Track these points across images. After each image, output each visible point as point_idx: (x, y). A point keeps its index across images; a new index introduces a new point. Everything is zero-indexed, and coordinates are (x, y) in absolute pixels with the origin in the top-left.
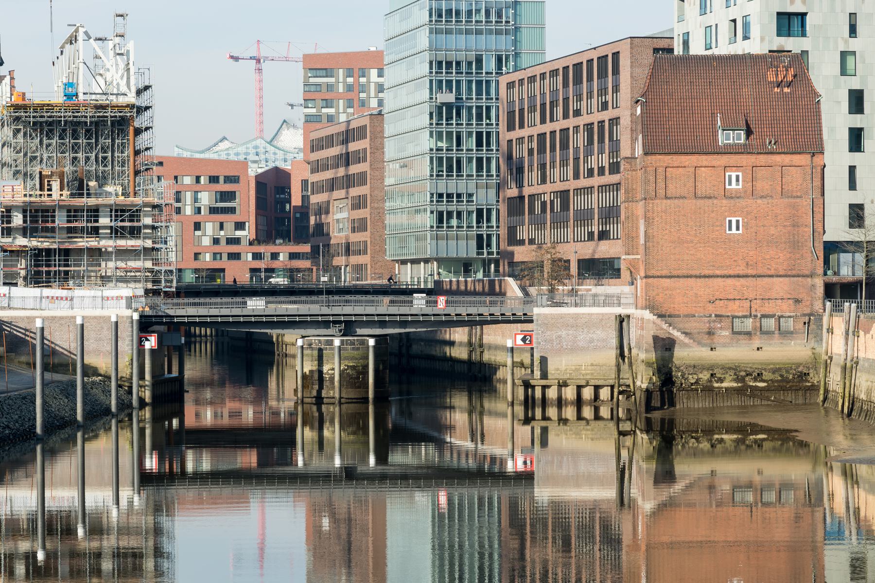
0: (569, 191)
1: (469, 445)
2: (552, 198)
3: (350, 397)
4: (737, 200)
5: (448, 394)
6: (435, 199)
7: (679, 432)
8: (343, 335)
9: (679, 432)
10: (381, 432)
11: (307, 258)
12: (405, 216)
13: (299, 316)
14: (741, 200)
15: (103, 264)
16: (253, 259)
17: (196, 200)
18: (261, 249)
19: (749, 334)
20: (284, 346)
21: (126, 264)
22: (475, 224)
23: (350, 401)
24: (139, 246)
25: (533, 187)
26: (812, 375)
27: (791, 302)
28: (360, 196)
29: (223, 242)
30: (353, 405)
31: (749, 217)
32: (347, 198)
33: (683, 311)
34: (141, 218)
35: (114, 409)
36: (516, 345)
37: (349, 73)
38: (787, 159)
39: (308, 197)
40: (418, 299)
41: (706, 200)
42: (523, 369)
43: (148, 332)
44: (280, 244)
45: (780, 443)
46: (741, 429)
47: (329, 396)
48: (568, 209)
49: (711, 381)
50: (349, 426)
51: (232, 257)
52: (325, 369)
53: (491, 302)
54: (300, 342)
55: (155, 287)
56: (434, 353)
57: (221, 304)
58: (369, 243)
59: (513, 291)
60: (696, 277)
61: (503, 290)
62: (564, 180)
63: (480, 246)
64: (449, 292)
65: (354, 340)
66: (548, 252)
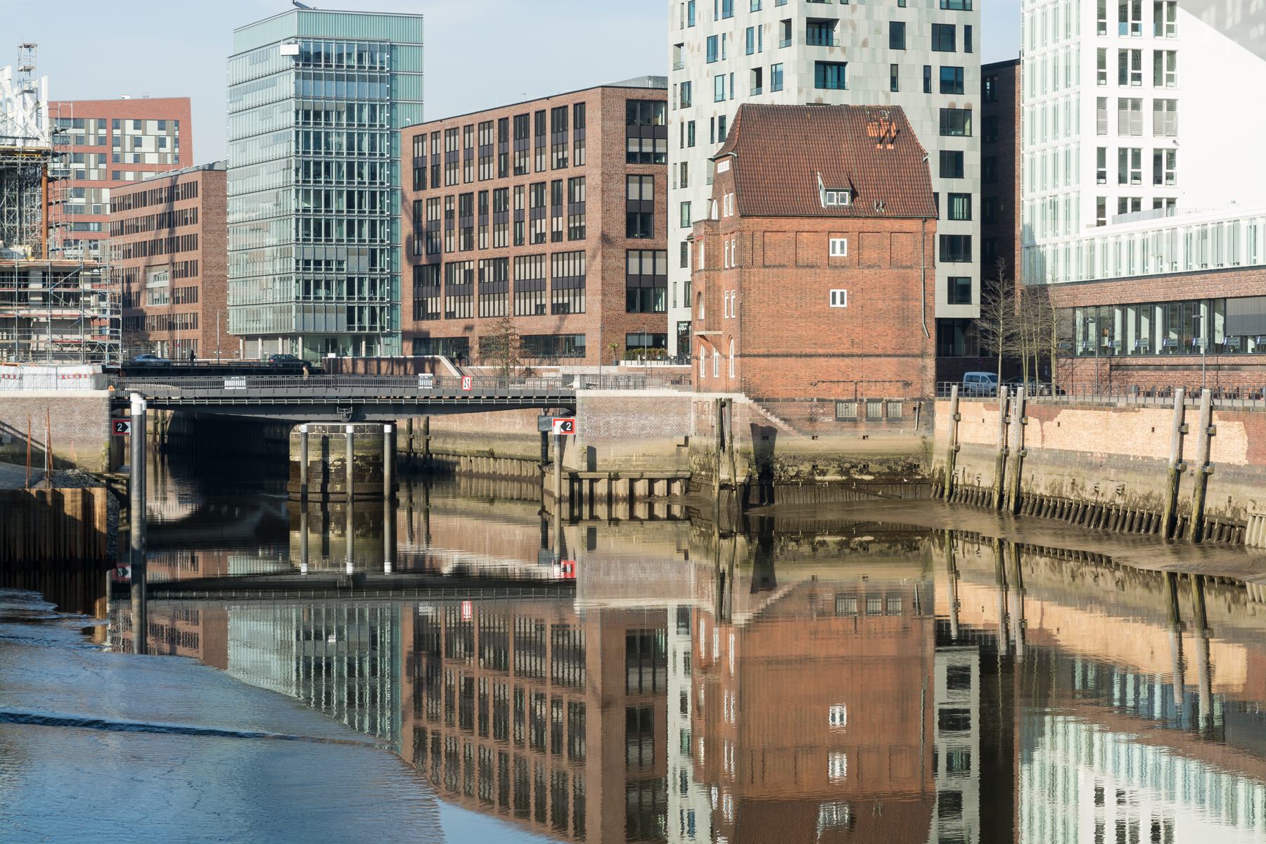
4: (842, 270)
6: (301, 266)
7: (777, 533)
9: (777, 533)
13: (235, 398)
14: (846, 270)
15: (34, 337)
19: (854, 420)
26: (922, 467)
27: (900, 385)
28: (186, 262)
31: (855, 289)
33: (781, 392)
37: (102, 124)
38: (896, 225)
40: (424, 379)
41: (808, 270)
45: (887, 545)
46: (847, 530)
49: (812, 474)
52: (332, 458)
58: (200, 316)
59: (447, 370)
60: (797, 356)
63: (350, 320)
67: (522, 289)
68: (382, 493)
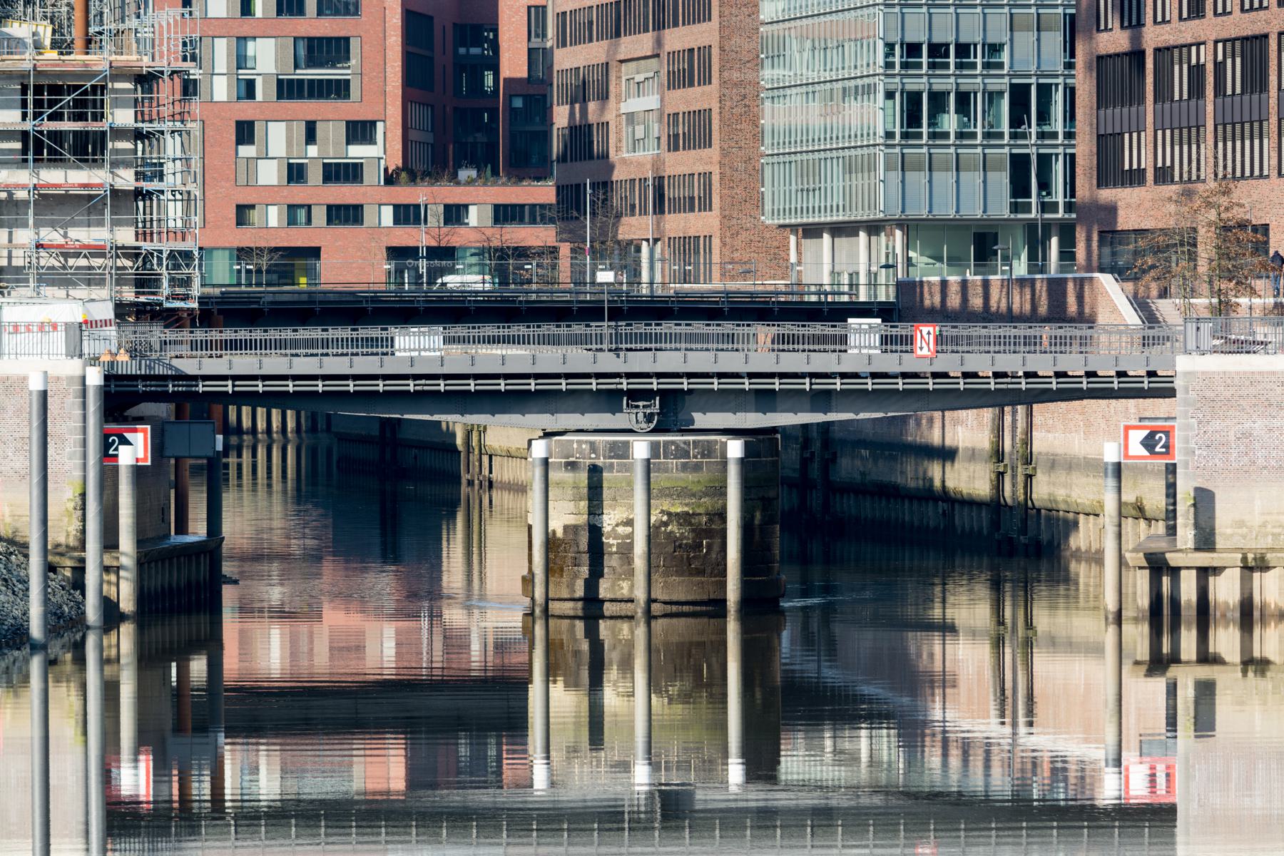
0: (1266, 36)
1: (988, 727)
2: (1220, 58)
3: (675, 598)
5: (938, 589)
6: (897, 60)
8: (654, 431)
10: (758, 695)
11: (544, 220)
12: (815, 106)
13: (477, 377)
16: (397, 221)
17: (241, 60)
18: (419, 194)
20: (485, 459)
21: (65, 236)
22: (1006, 128)
23: (674, 608)
24: (101, 185)
25: (1167, 27)
28: (691, 51)
29: (315, 175)
30: (683, 620)
32: (658, 56)
34: (107, 110)
35: (36, 630)
36: (1127, 456)
39: (547, 54)
42: (1142, 523)
43: (125, 420)
44: (470, 182)
47: (618, 596)
48: (1263, 87)
50: (672, 679)
51: (338, 217)
52: (609, 520)
53: (1055, 340)
54: (539, 449)
55: (142, 299)
56: (899, 480)
57: (325, 343)
58: (716, 179)
59: (1115, 310)
61: (1087, 310)
62: (1252, 9)
63: (1019, 188)
64: (940, 315)
65: (686, 443)
66: (1209, 205)
67: (1167, 124)
68: (724, 601)
